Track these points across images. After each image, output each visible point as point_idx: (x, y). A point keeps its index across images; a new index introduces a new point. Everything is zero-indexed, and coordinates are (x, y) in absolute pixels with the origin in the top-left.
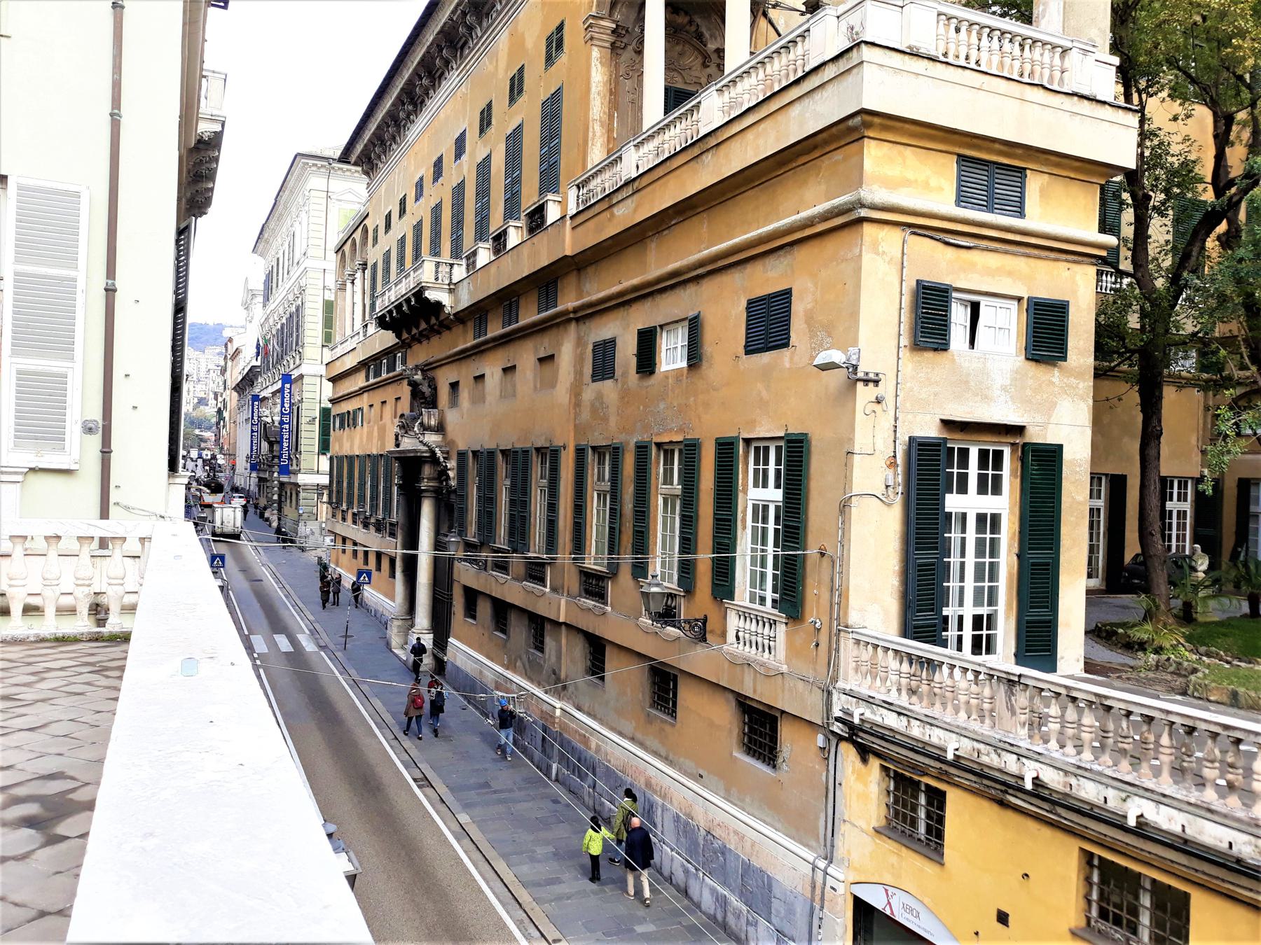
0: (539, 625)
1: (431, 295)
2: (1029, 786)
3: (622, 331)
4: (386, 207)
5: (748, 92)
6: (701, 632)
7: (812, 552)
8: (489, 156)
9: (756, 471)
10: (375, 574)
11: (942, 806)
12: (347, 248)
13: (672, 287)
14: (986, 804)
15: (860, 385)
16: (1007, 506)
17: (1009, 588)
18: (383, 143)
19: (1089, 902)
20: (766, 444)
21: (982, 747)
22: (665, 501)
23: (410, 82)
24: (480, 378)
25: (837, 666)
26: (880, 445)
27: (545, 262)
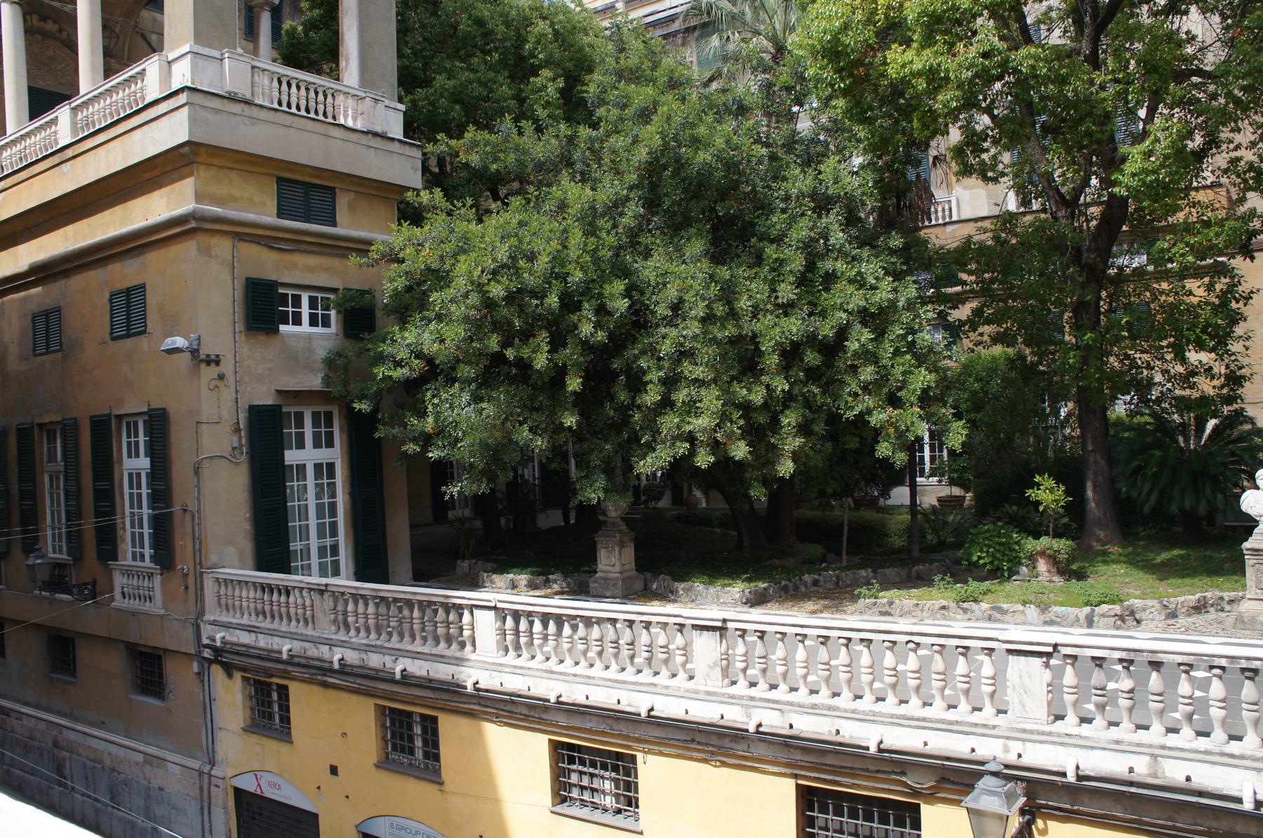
2: (336, 666)
6: (94, 591)
7: (176, 508)
9: (129, 444)
11: (435, 732)
14: (315, 689)
15: (203, 366)
17: (345, 521)
19: (386, 742)
21: (306, 644)
22: (51, 477)
25: (203, 602)
26: (225, 413)
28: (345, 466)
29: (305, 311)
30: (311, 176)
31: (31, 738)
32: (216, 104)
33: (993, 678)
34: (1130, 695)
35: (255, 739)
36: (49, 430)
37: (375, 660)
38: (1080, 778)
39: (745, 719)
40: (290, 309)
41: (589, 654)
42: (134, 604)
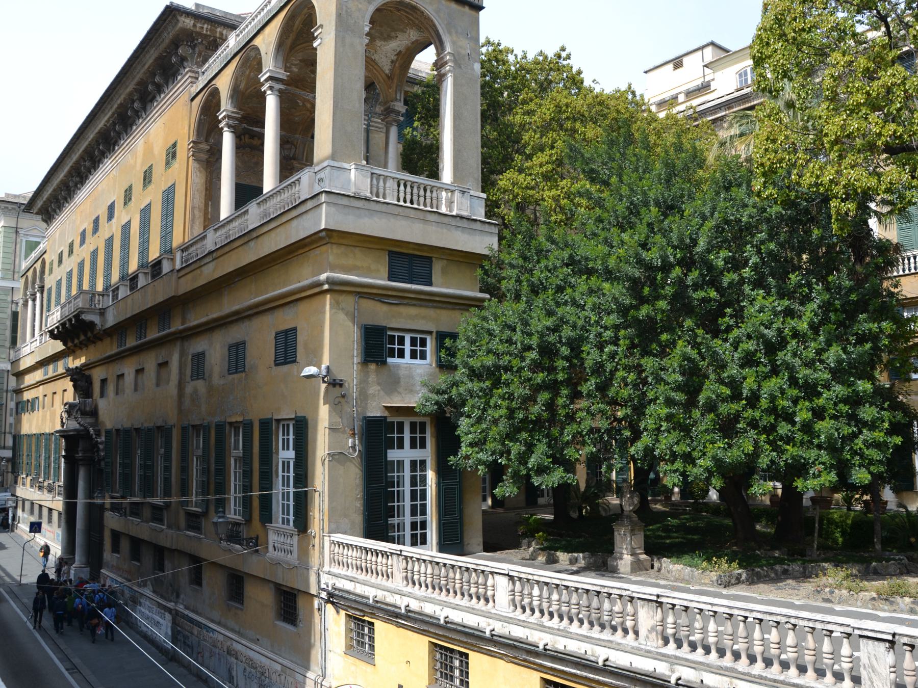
0: (160, 553)
1: (87, 317)
3: (215, 349)
4: (59, 247)
5: (273, 207)
6: (256, 543)
8: (129, 222)
9: (283, 439)
10: (44, 526)
12: (30, 274)
13: (237, 321)
16: (430, 455)
18: (57, 201)
20: (400, 419)
21: (386, 593)
22: (236, 461)
23: (77, 163)
24: (121, 376)
27: (161, 299)
28: (434, 463)
29: (407, 347)
30: (414, 249)
31: (214, 646)
32: (345, 201)
33: (778, 643)
34: (746, 640)
35: (351, 660)
36: (234, 425)
37: (429, 609)
38: (446, 622)
39: (667, 673)
40: (396, 346)
41: (580, 616)
42: (279, 555)
